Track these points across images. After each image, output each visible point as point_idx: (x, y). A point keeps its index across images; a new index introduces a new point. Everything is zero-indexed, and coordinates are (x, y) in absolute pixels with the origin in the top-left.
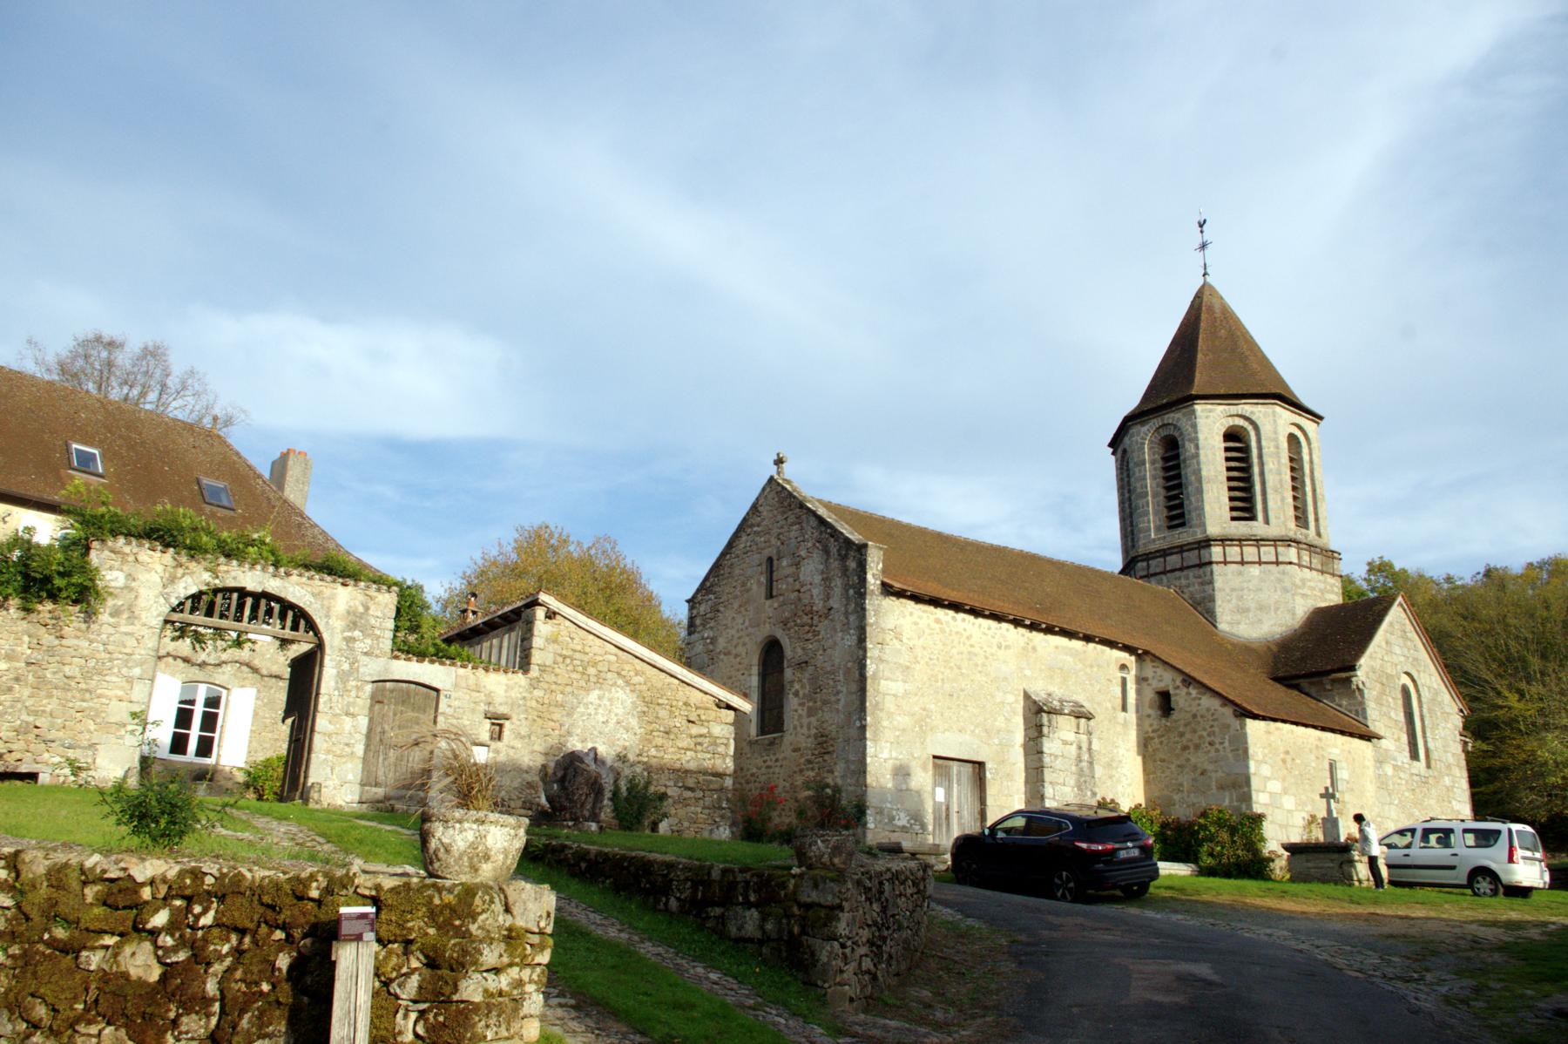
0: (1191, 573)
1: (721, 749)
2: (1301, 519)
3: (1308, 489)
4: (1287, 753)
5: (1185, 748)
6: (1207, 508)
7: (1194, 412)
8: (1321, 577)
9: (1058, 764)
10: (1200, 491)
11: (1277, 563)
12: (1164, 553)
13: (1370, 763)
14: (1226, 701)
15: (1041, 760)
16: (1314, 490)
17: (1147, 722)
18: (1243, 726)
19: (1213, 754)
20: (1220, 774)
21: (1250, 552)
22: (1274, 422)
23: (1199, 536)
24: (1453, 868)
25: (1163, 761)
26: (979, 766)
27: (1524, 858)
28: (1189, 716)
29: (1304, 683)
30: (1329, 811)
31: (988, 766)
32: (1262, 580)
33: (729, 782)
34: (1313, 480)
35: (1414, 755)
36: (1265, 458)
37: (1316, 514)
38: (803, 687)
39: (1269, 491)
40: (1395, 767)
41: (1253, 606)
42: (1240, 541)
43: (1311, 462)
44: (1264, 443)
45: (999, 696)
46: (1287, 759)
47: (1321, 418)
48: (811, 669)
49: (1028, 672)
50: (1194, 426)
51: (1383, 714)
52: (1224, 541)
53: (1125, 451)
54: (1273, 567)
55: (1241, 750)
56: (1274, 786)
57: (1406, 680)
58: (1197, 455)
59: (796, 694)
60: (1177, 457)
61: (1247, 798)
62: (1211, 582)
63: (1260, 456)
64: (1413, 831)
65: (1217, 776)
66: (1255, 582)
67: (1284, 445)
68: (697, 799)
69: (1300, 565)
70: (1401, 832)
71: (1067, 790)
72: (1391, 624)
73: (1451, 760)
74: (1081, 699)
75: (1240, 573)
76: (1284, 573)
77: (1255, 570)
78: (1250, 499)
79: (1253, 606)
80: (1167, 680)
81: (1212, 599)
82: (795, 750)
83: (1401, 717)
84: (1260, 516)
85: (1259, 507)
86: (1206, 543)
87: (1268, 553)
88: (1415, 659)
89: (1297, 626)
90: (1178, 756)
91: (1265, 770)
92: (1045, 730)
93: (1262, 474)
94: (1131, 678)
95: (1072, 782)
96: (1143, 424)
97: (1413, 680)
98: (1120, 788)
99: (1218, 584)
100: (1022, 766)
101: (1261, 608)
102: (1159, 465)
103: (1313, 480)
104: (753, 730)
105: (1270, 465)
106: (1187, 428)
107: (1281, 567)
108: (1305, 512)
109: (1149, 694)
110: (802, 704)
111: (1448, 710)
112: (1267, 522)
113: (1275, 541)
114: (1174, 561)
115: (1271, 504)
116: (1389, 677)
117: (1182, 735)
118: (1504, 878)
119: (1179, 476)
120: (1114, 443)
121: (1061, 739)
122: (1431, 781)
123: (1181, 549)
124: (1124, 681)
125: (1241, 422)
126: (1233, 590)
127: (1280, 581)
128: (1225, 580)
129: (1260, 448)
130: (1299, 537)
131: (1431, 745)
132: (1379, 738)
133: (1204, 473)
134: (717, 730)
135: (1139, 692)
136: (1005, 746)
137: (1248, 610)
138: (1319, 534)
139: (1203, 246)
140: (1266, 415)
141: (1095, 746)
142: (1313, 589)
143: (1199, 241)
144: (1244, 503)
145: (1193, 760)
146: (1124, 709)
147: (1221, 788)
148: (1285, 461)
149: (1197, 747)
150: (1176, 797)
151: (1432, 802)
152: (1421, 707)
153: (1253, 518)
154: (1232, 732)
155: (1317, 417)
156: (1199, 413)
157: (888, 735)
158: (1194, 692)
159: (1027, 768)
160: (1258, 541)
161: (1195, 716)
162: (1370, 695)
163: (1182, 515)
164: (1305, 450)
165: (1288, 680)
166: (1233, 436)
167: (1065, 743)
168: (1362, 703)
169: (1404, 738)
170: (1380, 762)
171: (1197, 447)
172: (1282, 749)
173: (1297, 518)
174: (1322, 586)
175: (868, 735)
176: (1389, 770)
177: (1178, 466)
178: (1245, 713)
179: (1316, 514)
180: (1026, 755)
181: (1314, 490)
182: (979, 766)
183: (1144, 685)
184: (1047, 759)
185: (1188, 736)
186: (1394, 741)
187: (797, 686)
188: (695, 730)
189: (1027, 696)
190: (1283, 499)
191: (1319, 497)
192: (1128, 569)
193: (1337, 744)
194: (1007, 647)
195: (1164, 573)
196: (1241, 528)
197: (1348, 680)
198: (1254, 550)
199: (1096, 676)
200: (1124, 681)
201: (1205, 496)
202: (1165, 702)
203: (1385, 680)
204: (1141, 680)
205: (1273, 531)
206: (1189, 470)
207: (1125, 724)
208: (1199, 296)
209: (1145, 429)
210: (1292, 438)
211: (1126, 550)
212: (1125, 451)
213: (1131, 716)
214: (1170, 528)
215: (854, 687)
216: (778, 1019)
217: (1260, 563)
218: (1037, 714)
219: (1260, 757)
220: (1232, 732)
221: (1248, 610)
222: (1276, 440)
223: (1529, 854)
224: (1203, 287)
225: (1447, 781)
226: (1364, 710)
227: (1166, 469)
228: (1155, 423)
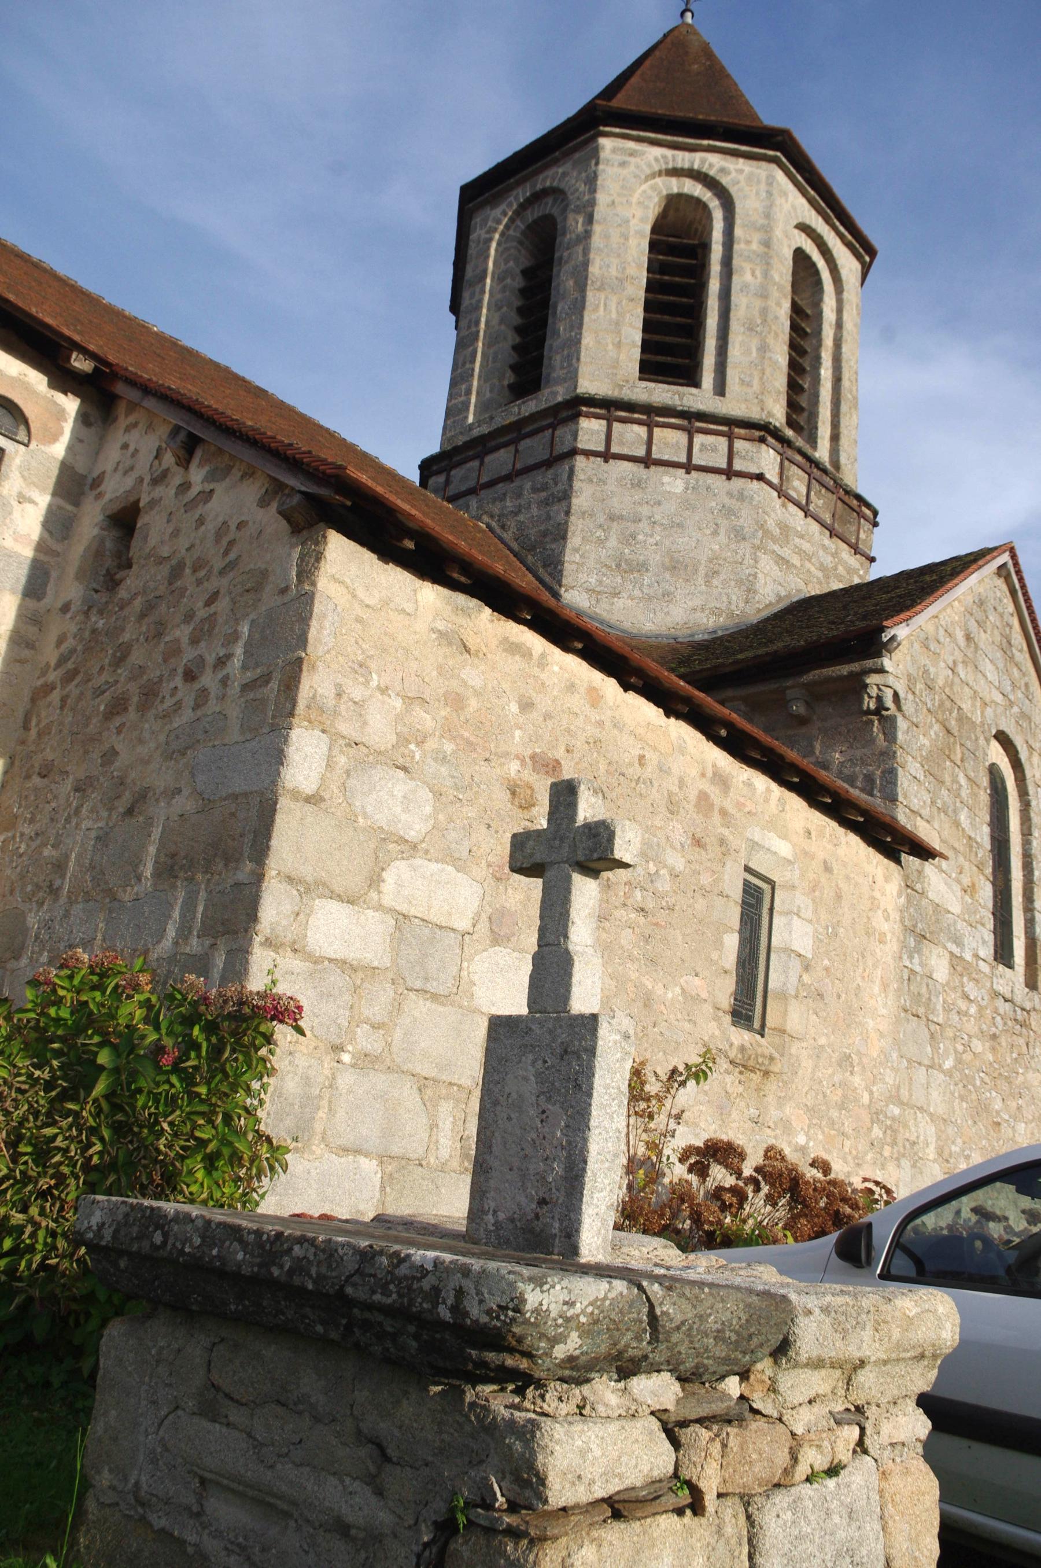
3: (826, 372)
6: (588, 340)
10: (579, 307)
11: (729, 473)
13: (889, 926)
16: (837, 380)
18: (309, 566)
21: (670, 441)
22: (766, 211)
30: (552, 968)
32: (687, 505)
34: (837, 360)
35: (1003, 954)
36: (736, 262)
37: (835, 425)
39: (735, 326)
40: (955, 961)
41: (655, 559)
42: (652, 415)
43: (839, 325)
44: (738, 232)
52: (611, 408)
54: (717, 482)
57: (997, 754)
61: (235, 918)
62: (566, 496)
69: (782, 493)
75: (638, 484)
76: (741, 497)
77: (675, 482)
79: (655, 559)
81: (561, 534)
83: (983, 835)
85: (709, 361)
86: (577, 405)
87: (710, 448)
93: (725, 295)
96: (494, 201)
97: (1017, 765)
99: (583, 498)
101: (675, 566)
103: (837, 360)
105: (745, 276)
107: (737, 483)
112: (720, 389)
113: (732, 426)
115: (734, 352)
125: (696, 189)
127: (729, 512)
128: (596, 491)
132: (924, 852)
133: (595, 270)
137: (642, 567)
142: (800, 552)
144: (674, 339)
155: (864, 250)
156: (605, 154)
160: (692, 421)
168: (888, 755)
169: (986, 892)
170: (920, 931)
171: (590, 219)
174: (828, 561)
179: (835, 425)
181: (837, 380)
190: (763, 349)
196: (661, 393)
197: (856, 686)
198: (680, 438)
201: (588, 317)
205: (732, 406)
206: (567, 268)
209: (497, 212)
217: (689, 467)
221: (642, 567)
222: (767, 230)
226: (890, 776)
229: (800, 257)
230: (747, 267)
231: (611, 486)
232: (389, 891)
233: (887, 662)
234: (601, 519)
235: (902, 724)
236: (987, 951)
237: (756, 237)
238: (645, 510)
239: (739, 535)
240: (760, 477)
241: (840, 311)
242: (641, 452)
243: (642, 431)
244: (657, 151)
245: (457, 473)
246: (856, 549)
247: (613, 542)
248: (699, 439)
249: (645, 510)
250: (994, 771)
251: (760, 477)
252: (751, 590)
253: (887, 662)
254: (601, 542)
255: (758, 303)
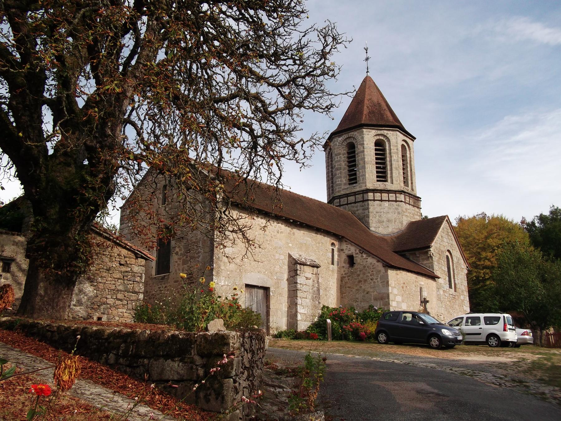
0: (359, 204)
1: (138, 279)
2: (406, 182)
3: (409, 169)
4: (404, 283)
5: (360, 281)
7: (363, 132)
8: (413, 208)
9: (304, 288)
10: (364, 167)
11: (396, 201)
12: (347, 195)
13: (435, 289)
14: (380, 260)
15: (296, 287)
16: (411, 170)
17: (343, 270)
18: (386, 271)
19: (372, 284)
20: (375, 293)
23: (363, 188)
24: (480, 334)
25: (349, 287)
26: (266, 290)
27: (510, 329)
28: (362, 266)
29: (407, 254)
31: (271, 289)
33: (141, 296)
34: (411, 165)
35: (450, 287)
37: (412, 180)
38: (180, 250)
41: (385, 220)
42: (381, 191)
44: (392, 147)
45: (277, 256)
46: (404, 286)
47: (415, 138)
48: (185, 241)
49: (290, 245)
50: (363, 138)
51: (439, 268)
52: (374, 191)
53: (330, 149)
55: (386, 284)
56: (399, 298)
57: (448, 254)
58: (363, 151)
59: (177, 253)
60: (354, 152)
62: (368, 209)
63: (390, 153)
64: (462, 318)
65: (374, 294)
66: (386, 209)
67: (400, 149)
68: (123, 305)
69: (405, 202)
70: (456, 319)
71: (308, 300)
72: (443, 229)
73: (463, 289)
74: (313, 258)
75: (380, 205)
76: (399, 206)
77: (386, 204)
78: (385, 173)
79: (385, 220)
80: (352, 250)
81: (368, 216)
82: (175, 282)
83: (446, 269)
84: (389, 180)
85: (389, 176)
87: (392, 196)
88: (452, 244)
89: (403, 229)
90: (356, 285)
91: (395, 291)
92: (298, 272)
93: (391, 161)
94: (336, 249)
95: (310, 297)
96: (339, 136)
98: (330, 300)
100: (286, 289)
101: (388, 221)
102: (346, 155)
104: (153, 272)
105: (394, 157)
106: (360, 138)
107: (398, 203)
108: (407, 179)
109: (344, 257)
110: (179, 259)
111: (463, 267)
113: (395, 192)
114: (352, 199)
115: (394, 174)
116: (442, 252)
117: (359, 275)
118: (502, 338)
119: (355, 161)
120: (326, 146)
121: (305, 277)
122: (456, 297)
123: (355, 194)
124: (333, 250)
125: (382, 138)
126: (377, 212)
128: (374, 208)
129: (390, 150)
130: (405, 190)
131: (456, 282)
134: (136, 269)
135: (339, 256)
136: (279, 280)
137: (383, 222)
138: (413, 190)
139: (367, 59)
140: (393, 135)
141: (320, 281)
143: (365, 57)
144: (382, 175)
145: (363, 287)
146: (333, 264)
147: (376, 299)
148: (400, 156)
149: (365, 281)
150: (355, 304)
151: (457, 306)
152: (453, 265)
153: (386, 181)
154: (382, 274)
157: (224, 273)
158: (365, 256)
159: (289, 291)
160: (389, 192)
161: (365, 267)
162: (435, 259)
163: (356, 179)
164: (408, 152)
165: (401, 253)
166: (379, 144)
167: (307, 278)
170: (438, 289)
172: (402, 282)
173: (404, 182)
174: (414, 212)
175: (214, 273)
176: (441, 292)
177: (354, 157)
178: (390, 266)
179: (412, 180)
180: (289, 284)
181: (411, 170)
182: (266, 290)
183: (342, 252)
184: (299, 286)
185: (361, 276)
186: (443, 280)
187: (177, 249)
188: (124, 269)
189: (290, 256)
190: (399, 173)
191: (413, 173)
192: (330, 201)
193: (423, 281)
194: (281, 232)
195: (347, 204)
199: (317, 248)
200: (333, 250)
202: (351, 260)
203: (440, 253)
204: (340, 250)
207: (333, 271)
208: (365, 81)
209: (340, 139)
210: (403, 146)
211: (329, 195)
212: (330, 149)
213: (335, 267)
214: (349, 184)
215: (207, 250)
216: (93, 392)
217: (389, 201)
218: (294, 266)
219: (393, 285)
220: (382, 274)
221: (383, 222)
222: (397, 146)
223: (511, 327)
224: (367, 77)
225: (462, 297)
227: (349, 158)
228: (345, 136)
229: (403, 145)
230: (394, 155)
231: (376, 206)
232: (396, 300)
233: (431, 249)
234: (375, 213)
235: (434, 257)
236: (448, 288)
237: (395, 148)
238: (382, 210)
239: (399, 213)
240: (402, 201)
241: (410, 154)
242: (380, 199)
243: (379, 194)
244: (374, 131)
245: (342, 200)
246: (418, 208)
247: (377, 217)
248: (390, 195)
249: (382, 210)
250: (447, 256)
251: (402, 201)
252: (402, 224)
253: (431, 249)
254: (375, 217)
255: (397, 163)
